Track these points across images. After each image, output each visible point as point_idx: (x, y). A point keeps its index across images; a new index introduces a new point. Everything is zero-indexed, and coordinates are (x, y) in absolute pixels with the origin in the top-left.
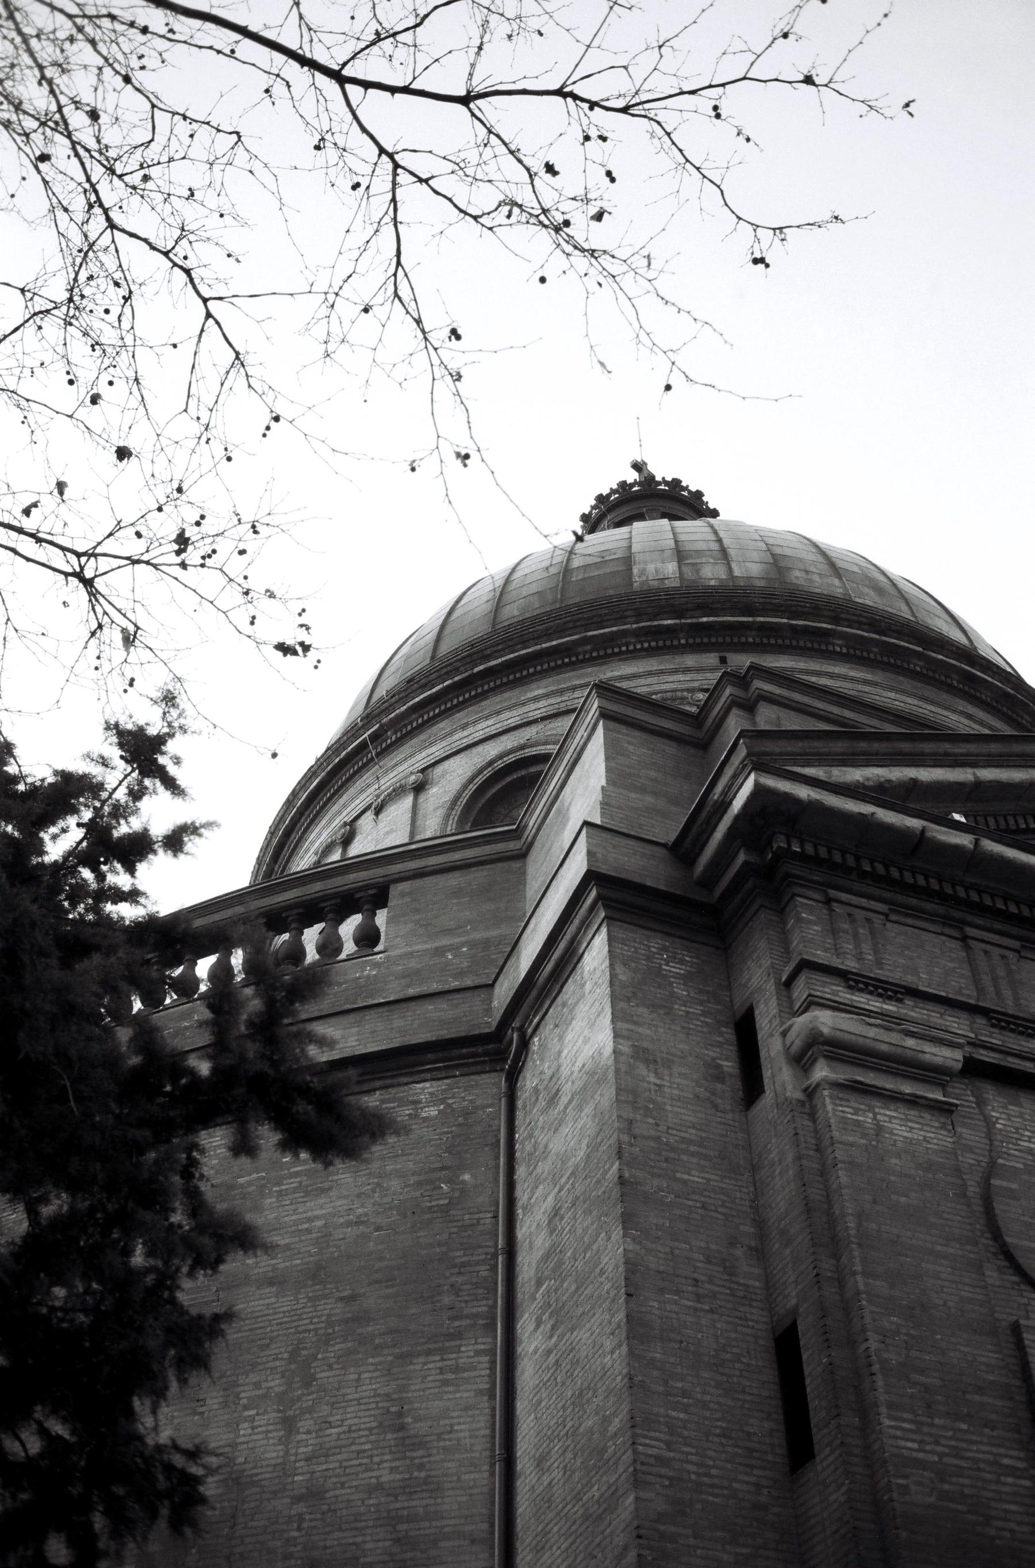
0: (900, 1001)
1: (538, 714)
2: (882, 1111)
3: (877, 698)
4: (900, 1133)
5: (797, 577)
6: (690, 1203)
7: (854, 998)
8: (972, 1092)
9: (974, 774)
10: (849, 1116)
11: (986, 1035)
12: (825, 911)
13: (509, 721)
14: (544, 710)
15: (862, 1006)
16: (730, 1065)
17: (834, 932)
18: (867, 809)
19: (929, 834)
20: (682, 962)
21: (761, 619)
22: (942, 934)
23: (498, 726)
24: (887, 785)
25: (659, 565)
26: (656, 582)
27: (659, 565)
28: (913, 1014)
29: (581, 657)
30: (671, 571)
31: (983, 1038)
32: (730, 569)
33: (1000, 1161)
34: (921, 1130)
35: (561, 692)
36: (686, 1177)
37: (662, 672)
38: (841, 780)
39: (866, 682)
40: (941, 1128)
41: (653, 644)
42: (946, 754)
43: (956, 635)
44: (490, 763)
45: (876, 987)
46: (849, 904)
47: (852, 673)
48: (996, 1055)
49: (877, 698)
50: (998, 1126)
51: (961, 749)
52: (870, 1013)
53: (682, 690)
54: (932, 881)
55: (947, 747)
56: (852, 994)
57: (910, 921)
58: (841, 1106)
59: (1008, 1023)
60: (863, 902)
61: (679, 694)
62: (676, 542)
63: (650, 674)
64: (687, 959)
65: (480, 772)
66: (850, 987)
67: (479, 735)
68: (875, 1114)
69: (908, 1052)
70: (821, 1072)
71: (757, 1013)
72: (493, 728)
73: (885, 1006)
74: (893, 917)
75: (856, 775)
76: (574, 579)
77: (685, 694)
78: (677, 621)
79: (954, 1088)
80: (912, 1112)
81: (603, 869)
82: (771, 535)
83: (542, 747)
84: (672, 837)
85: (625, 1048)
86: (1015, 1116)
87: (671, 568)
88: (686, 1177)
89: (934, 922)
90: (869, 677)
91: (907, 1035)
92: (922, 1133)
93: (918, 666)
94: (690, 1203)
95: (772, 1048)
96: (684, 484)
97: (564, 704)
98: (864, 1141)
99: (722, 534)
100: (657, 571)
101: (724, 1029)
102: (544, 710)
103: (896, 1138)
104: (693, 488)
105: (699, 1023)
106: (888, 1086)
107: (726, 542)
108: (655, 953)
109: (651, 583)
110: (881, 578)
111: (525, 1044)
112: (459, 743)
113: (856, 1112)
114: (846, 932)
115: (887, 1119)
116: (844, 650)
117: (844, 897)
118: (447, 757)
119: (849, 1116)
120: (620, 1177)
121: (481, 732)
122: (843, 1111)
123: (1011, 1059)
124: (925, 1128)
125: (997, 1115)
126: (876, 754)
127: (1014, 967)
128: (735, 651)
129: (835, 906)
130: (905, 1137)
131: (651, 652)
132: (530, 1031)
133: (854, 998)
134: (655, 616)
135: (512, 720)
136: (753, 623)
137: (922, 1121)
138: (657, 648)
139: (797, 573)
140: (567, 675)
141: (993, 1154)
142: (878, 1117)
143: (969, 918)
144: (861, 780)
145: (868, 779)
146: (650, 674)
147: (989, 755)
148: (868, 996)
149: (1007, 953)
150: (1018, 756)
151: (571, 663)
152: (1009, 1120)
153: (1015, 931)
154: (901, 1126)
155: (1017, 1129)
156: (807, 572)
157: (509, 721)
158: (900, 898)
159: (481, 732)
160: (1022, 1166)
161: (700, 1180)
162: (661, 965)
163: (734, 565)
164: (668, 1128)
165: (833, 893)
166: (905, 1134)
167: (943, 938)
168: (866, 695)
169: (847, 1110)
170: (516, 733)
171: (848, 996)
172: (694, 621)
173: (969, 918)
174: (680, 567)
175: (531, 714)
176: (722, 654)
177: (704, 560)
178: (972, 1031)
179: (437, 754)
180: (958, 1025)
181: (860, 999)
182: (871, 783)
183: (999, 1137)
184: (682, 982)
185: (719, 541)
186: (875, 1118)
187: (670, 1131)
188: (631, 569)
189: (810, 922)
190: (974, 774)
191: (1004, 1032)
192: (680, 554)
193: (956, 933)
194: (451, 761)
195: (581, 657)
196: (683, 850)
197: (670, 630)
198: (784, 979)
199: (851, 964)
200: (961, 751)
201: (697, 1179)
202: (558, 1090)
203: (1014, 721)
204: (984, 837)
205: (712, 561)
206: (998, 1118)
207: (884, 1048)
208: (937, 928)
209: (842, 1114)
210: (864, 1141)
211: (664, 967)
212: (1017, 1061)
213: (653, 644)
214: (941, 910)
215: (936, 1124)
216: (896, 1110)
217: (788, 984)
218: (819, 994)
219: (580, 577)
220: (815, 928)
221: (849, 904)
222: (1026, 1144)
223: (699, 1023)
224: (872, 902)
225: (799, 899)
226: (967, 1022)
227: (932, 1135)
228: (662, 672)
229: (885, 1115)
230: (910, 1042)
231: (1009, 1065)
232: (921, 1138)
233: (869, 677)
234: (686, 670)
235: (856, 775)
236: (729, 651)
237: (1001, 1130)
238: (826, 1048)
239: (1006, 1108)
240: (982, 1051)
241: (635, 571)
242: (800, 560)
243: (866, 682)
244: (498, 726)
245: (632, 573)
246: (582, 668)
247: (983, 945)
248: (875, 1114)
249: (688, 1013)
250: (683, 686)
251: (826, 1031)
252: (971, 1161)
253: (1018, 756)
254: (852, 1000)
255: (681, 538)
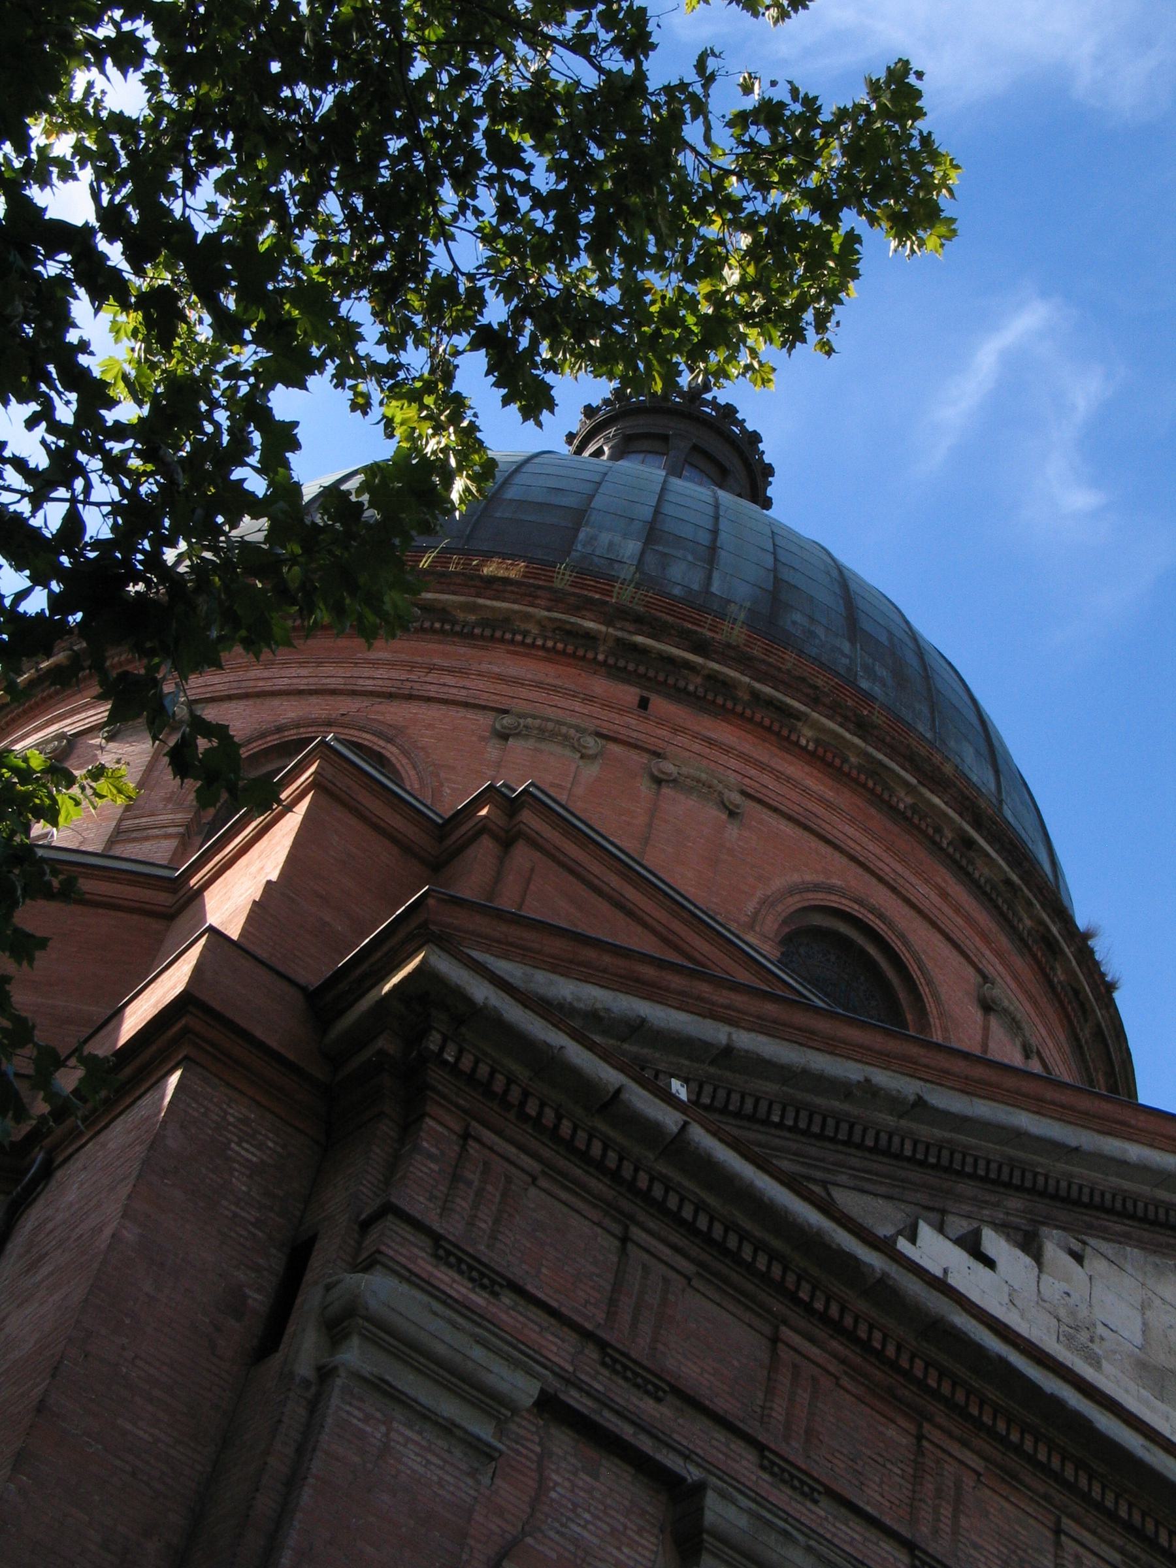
0: (495, 1295)
1: (369, 685)
2: (402, 1429)
3: (828, 827)
4: (410, 1463)
5: (794, 623)
6: (118, 1462)
7: (436, 1272)
8: (541, 1438)
9: (730, 1034)
10: (355, 1421)
11: (587, 1373)
12: (456, 1148)
13: (328, 681)
14: (380, 682)
15: (442, 1286)
16: (258, 1300)
17: (456, 1178)
18: (556, 1038)
19: (625, 1096)
20: (260, 1146)
21: (716, 666)
22: (599, 1224)
23: (311, 680)
24: (602, 1014)
25: (617, 539)
26: (603, 561)
27: (617, 539)
28: (504, 1317)
29: (458, 628)
30: (628, 553)
31: (583, 1377)
32: (709, 578)
33: (529, 1540)
34: (442, 1468)
35: (412, 667)
36: (129, 1427)
37: (555, 689)
38: (542, 991)
39: (821, 800)
40: (468, 1474)
41: (560, 646)
42: (700, 998)
43: (980, 775)
44: (279, 729)
45: (471, 1268)
46: (491, 1149)
47: (809, 782)
48: (589, 1403)
49: (828, 827)
50: (553, 1495)
51: (723, 997)
52: (446, 1300)
53: (571, 726)
54: (611, 1154)
55: (705, 988)
56: (436, 1267)
57: (564, 1195)
58: (350, 1404)
59: (626, 1367)
60: (512, 1151)
61: (564, 730)
62: (657, 511)
63: (539, 685)
64: (270, 1144)
65: (263, 735)
66: (436, 1256)
67: (282, 683)
68: (389, 1430)
69: (470, 1365)
70: (354, 1355)
71: (317, 1246)
72: (305, 681)
73: (473, 1296)
74: (543, 1183)
75: (565, 989)
76: (498, 515)
77: (572, 732)
78: (603, 628)
79: (520, 1426)
80: (440, 1442)
81: (204, 996)
82: (794, 549)
83: (356, 733)
84: (313, 980)
85: (130, 1235)
86: (582, 1489)
87: (631, 548)
88: (129, 1427)
89: (595, 1206)
90: (830, 795)
91: (478, 1342)
92: (440, 1472)
93: (904, 800)
94: (118, 1462)
95: (310, 1299)
96: (739, 416)
97: (409, 684)
98: (357, 1459)
99: (724, 525)
100: (611, 544)
101: (273, 1251)
102: (380, 682)
103: (403, 1468)
104: (750, 427)
105: (244, 1233)
106: (423, 1400)
107: (723, 537)
108: (229, 1124)
109: (596, 559)
110: (913, 661)
111: (47, 1172)
112: (251, 683)
113: (367, 1418)
114: (469, 1183)
115: (401, 1440)
116: (811, 747)
117: (488, 1136)
118: (229, 698)
119: (355, 1421)
120: (41, 1401)
121: (286, 681)
122: (348, 1413)
123: (607, 1414)
124: (447, 1467)
125: (559, 1480)
126: (605, 971)
127: (672, 1298)
128: (668, 696)
129: (473, 1147)
130: (414, 1471)
131: (552, 655)
132: (60, 1159)
133: (436, 1272)
134: (576, 610)
135: (333, 680)
136: (703, 667)
137: (446, 1455)
138: (563, 653)
139: (798, 617)
140: (430, 646)
141: (527, 1528)
142: (393, 1435)
143: (641, 1217)
144: (569, 998)
145: (579, 999)
146: (539, 685)
147: (758, 1017)
148: (457, 1277)
149: (672, 1275)
150: (799, 1029)
151: (442, 631)
152: (572, 1491)
153: (694, 1251)
154: (417, 1454)
155: (575, 1505)
156: (812, 619)
157: (328, 681)
158: (562, 1163)
159: (286, 681)
160: (554, 1556)
161: (146, 1436)
162: (230, 1141)
163: (716, 575)
164: (136, 1357)
165: (476, 1128)
166: (416, 1467)
167: (599, 1230)
168: (814, 819)
169: (356, 1413)
170: (331, 700)
171: (430, 1268)
172: (625, 635)
173: (641, 1217)
174: (643, 553)
175: (361, 682)
176: (645, 694)
177: (679, 553)
178: (572, 1363)
179: (219, 687)
180: (558, 1348)
181: (444, 1277)
182: (582, 1005)
183: (546, 1509)
184: (248, 1172)
185: (715, 532)
186: (387, 1435)
187: (139, 1363)
188: (578, 530)
189: (430, 1156)
190: (730, 1034)
191: (614, 1377)
192: (654, 532)
193: (617, 1229)
194: (233, 704)
195: (458, 628)
196: (325, 1001)
197: (590, 638)
198: (363, 1217)
199: (452, 1228)
200: (721, 1000)
201: (141, 1433)
202: (47, 1254)
203: (1006, 919)
204: (698, 1123)
205: (690, 558)
206: (556, 1484)
207: (440, 1349)
208: (595, 1215)
209: (344, 1415)
210: (357, 1459)
211: (233, 1145)
212: (614, 1418)
213: (560, 646)
214: (610, 1194)
215: (464, 1467)
216: (420, 1433)
217: (365, 1226)
218: (391, 1253)
219: (507, 515)
220: (432, 1166)
221: (491, 1149)
222: (578, 1529)
223: (244, 1233)
224: (523, 1156)
225: (431, 1123)
226: (572, 1350)
227: (451, 1480)
228: (555, 689)
229: (402, 1434)
230: (478, 1353)
231: (601, 1421)
232: (435, 1478)
233: (830, 795)
234: (589, 699)
235: (565, 989)
236: (658, 692)
237: (552, 1500)
238: (366, 1324)
239: (575, 1474)
240: (574, 1393)
241: (582, 536)
242: (811, 599)
243: (821, 800)
244: (311, 680)
245: (576, 536)
246: (454, 643)
247: (646, 1256)
248: (389, 1430)
249: (235, 1215)
250: (574, 721)
251: (373, 1304)
252: (494, 1528)
253: (799, 1029)
254: (431, 1274)
255: (668, 509)
